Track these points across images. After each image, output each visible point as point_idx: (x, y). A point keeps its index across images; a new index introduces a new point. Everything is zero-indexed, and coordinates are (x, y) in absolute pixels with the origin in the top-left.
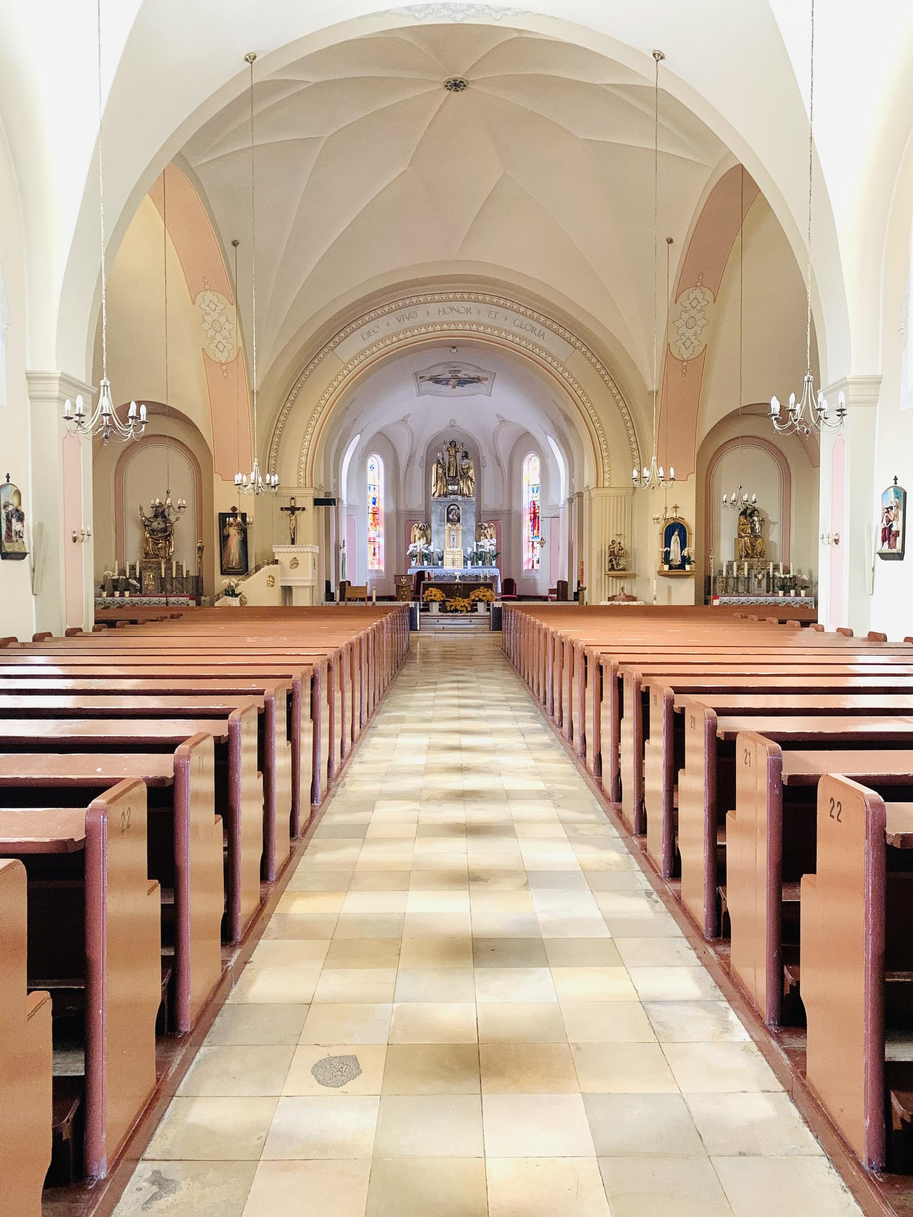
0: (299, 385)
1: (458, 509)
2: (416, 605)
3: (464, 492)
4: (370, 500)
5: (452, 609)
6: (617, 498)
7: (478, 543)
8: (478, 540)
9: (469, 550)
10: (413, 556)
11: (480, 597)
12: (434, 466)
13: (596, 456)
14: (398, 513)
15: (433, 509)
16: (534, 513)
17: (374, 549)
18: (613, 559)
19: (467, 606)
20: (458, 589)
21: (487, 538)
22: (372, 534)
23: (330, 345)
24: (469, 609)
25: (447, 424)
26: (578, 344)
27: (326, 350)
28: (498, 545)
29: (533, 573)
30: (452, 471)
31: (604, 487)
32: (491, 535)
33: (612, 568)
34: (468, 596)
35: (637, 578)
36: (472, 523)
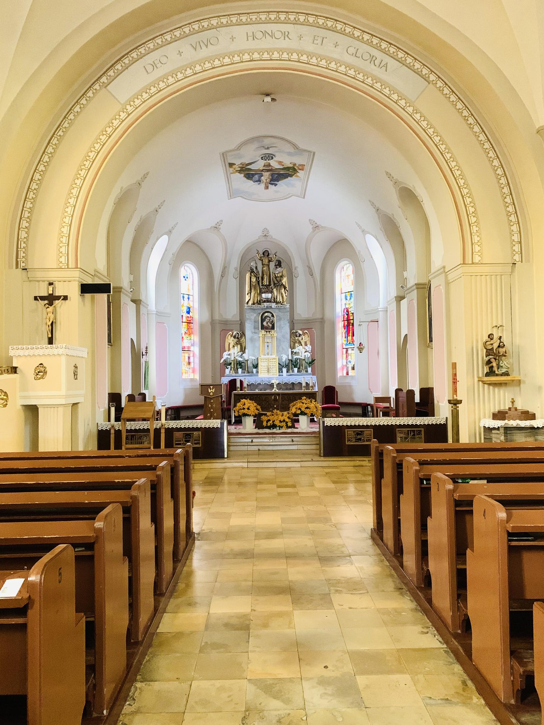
0: (61, 133)
1: (273, 316)
2: (222, 424)
3: (278, 300)
4: (185, 309)
5: (269, 425)
6: (496, 278)
7: (294, 350)
8: (292, 347)
9: (284, 358)
10: (227, 364)
11: (303, 409)
12: (248, 275)
13: (461, 225)
14: (213, 322)
15: (247, 317)
16: (348, 320)
17: (189, 358)
18: (493, 360)
19: (287, 420)
20: (275, 400)
21: (301, 345)
22: (186, 343)
23: (102, 80)
24: (290, 424)
25: (260, 233)
26: (432, 77)
27: (97, 86)
28: (313, 351)
29: (348, 380)
30: (265, 280)
31: (473, 263)
32: (306, 342)
33: (491, 373)
34: (287, 408)
35: (522, 385)
36: (286, 329)
